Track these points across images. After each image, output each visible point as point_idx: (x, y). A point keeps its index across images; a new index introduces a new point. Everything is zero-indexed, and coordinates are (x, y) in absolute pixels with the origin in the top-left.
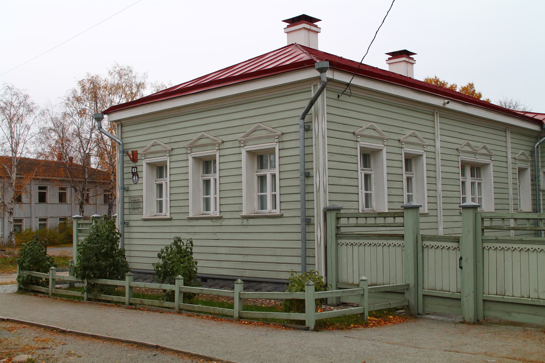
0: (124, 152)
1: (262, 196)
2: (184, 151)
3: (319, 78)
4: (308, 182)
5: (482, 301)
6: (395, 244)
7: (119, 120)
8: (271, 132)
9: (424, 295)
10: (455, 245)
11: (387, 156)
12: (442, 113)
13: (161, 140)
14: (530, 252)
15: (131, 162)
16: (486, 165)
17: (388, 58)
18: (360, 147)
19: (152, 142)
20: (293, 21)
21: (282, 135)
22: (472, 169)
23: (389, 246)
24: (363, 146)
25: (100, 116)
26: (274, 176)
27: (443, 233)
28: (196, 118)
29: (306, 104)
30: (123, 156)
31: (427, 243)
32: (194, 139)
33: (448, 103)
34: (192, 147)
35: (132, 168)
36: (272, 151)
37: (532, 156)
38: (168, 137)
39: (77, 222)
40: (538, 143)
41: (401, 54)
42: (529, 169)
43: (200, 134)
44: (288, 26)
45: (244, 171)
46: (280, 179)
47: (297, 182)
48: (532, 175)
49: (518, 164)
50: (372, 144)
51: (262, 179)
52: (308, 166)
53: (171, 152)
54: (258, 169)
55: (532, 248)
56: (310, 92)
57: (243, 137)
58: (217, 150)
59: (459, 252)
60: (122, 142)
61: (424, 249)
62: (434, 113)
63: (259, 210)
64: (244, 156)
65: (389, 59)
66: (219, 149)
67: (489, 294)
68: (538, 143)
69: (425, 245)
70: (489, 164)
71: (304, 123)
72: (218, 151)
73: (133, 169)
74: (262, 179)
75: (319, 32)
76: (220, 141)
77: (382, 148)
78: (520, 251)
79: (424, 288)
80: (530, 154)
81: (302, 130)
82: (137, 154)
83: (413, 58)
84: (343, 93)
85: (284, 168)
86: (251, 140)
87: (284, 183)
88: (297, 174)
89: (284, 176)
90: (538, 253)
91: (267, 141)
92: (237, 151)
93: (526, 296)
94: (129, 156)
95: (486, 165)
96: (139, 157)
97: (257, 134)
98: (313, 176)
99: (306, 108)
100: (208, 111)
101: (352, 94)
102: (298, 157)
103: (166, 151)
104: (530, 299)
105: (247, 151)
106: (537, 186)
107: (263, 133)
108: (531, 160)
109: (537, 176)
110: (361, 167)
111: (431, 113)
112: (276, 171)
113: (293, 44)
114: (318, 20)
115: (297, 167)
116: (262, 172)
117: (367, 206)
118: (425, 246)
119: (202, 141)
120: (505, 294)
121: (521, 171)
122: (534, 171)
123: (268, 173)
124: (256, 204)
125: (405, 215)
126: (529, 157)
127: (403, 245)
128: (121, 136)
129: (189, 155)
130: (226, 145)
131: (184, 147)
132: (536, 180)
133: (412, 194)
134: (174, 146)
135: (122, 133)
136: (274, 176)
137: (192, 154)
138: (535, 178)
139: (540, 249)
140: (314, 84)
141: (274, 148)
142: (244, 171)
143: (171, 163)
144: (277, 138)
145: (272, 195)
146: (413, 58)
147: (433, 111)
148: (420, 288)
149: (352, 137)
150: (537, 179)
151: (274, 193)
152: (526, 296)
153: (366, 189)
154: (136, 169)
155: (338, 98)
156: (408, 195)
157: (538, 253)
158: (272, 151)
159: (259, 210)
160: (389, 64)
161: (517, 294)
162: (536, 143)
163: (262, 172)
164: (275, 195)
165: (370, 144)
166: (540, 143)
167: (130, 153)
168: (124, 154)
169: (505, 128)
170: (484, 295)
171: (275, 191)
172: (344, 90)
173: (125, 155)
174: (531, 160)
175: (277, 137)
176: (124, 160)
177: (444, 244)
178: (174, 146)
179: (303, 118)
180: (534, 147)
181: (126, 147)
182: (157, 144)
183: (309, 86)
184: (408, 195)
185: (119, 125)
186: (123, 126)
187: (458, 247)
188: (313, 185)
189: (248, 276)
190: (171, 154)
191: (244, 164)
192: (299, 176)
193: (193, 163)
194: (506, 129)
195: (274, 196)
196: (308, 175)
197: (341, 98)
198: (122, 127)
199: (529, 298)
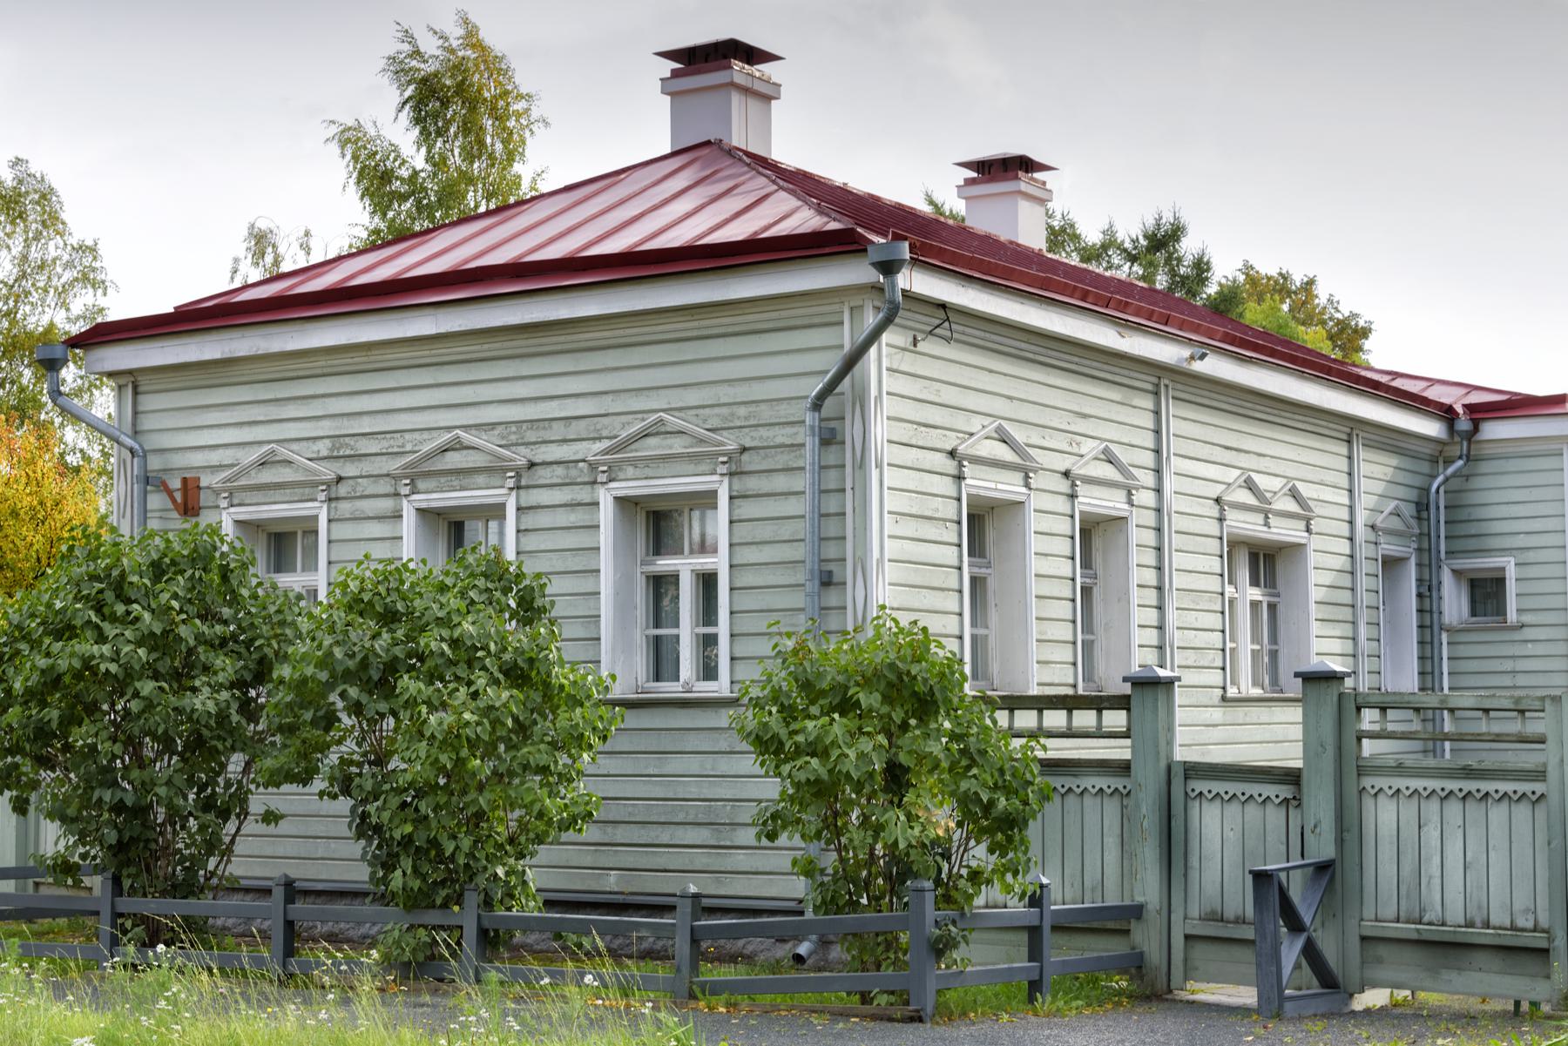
0: (147, 481)
1: (657, 640)
2: (384, 487)
3: (877, 289)
4: (832, 598)
5: (1357, 940)
6: (1201, 793)
7: (130, 372)
8: (701, 441)
9: (1187, 937)
10: (1285, 791)
12: (1179, 386)
13: (295, 447)
14: (1490, 801)
15: (175, 515)
17: (966, 180)
19: (255, 454)
21: (741, 453)
22: (1254, 558)
23: (1082, 793)
25: (58, 352)
26: (707, 582)
28: (431, 381)
29: (832, 362)
30: (146, 493)
31: (1200, 786)
32: (426, 448)
33: (1202, 357)
34: (415, 476)
37: (1419, 518)
38: (322, 438)
40: (1440, 479)
41: (1006, 170)
42: (1413, 561)
43: (447, 436)
44: (675, 74)
45: (606, 561)
46: (731, 589)
47: (797, 599)
48: (1420, 581)
50: (1000, 486)
51: (661, 586)
52: (831, 551)
53: (334, 488)
54: (647, 554)
55: (1533, 793)
56: (836, 328)
57: (607, 454)
58: (511, 489)
59: (1299, 811)
60: (141, 446)
61: (1190, 803)
62: (1157, 385)
63: (648, 681)
66: (519, 488)
67: (1376, 920)
68: (1440, 479)
69: (1193, 790)
71: (821, 420)
72: (514, 493)
74: (661, 586)
75: (777, 98)
76: (522, 462)
77: (1022, 498)
78: (1464, 798)
79: (1189, 915)
80: (1415, 514)
81: (811, 443)
82: (199, 488)
83: (1044, 183)
84: (930, 332)
85: (748, 555)
86: (634, 462)
87: (747, 601)
88: (800, 576)
89: (747, 579)
90: (1513, 804)
91: (691, 468)
92: (583, 494)
93: (1478, 921)
94: (170, 493)
96: (205, 498)
97: (653, 446)
98: (845, 583)
99: (829, 376)
100: (479, 364)
101: (955, 335)
102: (799, 524)
103: (315, 484)
104: (1491, 931)
105: (616, 499)
106: (1435, 616)
107: (677, 445)
108: (1417, 531)
109: (1434, 582)
111: (1150, 387)
112: (719, 562)
113: (708, 143)
114: (767, 57)
115: (798, 552)
116: (665, 564)
118: (1193, 795)
119: (454, 460)
120: (1421, 918)
121: (1391, 564)
122: (1427, 570)
123: (684, 566)
124: (640, 664)
125: (1133, 703)
126: (1414, 522)
127: (1125, 792)
128: (134, 424)
129: (405, 502)
130: (544, 475)
131: (388, 475)
132: (1431, 597)
134: (350, 470)
135: (136, 413)
136: (707, 582)
137: (415, 497)
138: (1430, 589)
139: (1519, 794)
140: (852, 304)
142: (606, 561)
143: (333, 525)
144: (723, 463)
145: (697, 635)
146: (1044, 183)
148: (1177, 917)
150: (1434, 594)
152: (1478, 921)
155: (915, 345)
157: (1513, 804)
159: (648, 681)
161: (1455, 915)
162: (1434, 477)
163: (665, 564)
165: (992, 485)
166: (1447, 480)
167: (176, 484)
168: (149, 488)
169: (1348, 430)
170: (1363, 923)
172: (938, 322)
173: (152, 492)
174: (1417, 531)
175: (725, 459)
176: (149, 507)
177: (1253, 789)
178: (350, 470)
179: (818, 404)
180: (1428, 490)
181: (155, 463)
182: (277, 458)
183: (836, 307)
185: (126, 385)
186: (141, 389)
187: (1294, 798)
188: (845, 608)
189: (616, 889)
190: (333, 496)
191: (606, 537)
192: (802, 581)
193: (417, 527)
194: (1349, 435)
195: (709, 642)
196: (827, 581)
197: (921, 347)
198: (136, 393)
199: (1488, 928)
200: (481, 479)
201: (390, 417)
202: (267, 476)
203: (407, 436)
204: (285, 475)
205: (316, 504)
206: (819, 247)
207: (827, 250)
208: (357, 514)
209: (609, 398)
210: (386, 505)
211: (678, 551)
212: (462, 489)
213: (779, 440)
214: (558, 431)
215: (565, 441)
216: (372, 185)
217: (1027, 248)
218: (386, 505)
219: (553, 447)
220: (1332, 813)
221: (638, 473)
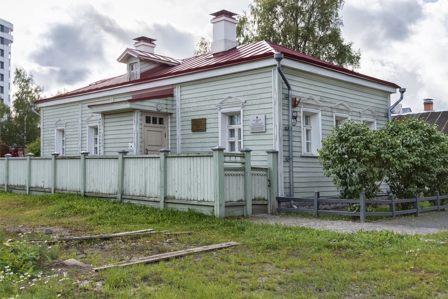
11: (322, 117)
16: (316, 114)
18: (303, 111)
19: (308, 96)
20: (218, 14)
24: (337, 115)
27: (283, 170)
35: (293, 112)
36: (238, 114)
39: (123, 156)
49: (336, 113)
54: (229, 125)
64: (220, 115)
65: (214, 19)
70: (373, 122)
73: (294, 113)
95: (316, 114)
110: (303, 124)
112: (241, 126)
116: (233, 127)
117: (308, 151)
133: (310, 142)
136: (240, 130)
141: (240, 111)
147: (387, 95)
149: (330, 110)
151: (239, 141)
153: (307, 139)
154: (296, 113)
156: (307, 142)
158: (238, 114)
160: (213, 23)
163: (233, 127)
164: (240, 142)
171: (240, 139)
184: (307, 142)
191: (220, 120)
200: (345, 112)
201: (331, 95)
202: (309, 102)
203: (333, 100)
204: (312, 102)
205: (319, 111)
206: (227, 64)
207: (225, 65)
208: (325, 115)
209: (361, 101)
210: (330, 114)
211: (234, 124)
212: (342, 113)
213: (381, 115)
214: (355, 105)
215: (356, 108)
216: (262, 8)
217: (124, 63)
218: (330, 114)
219: (354, 108)
220: (28, 169)
221: (366, 116)
